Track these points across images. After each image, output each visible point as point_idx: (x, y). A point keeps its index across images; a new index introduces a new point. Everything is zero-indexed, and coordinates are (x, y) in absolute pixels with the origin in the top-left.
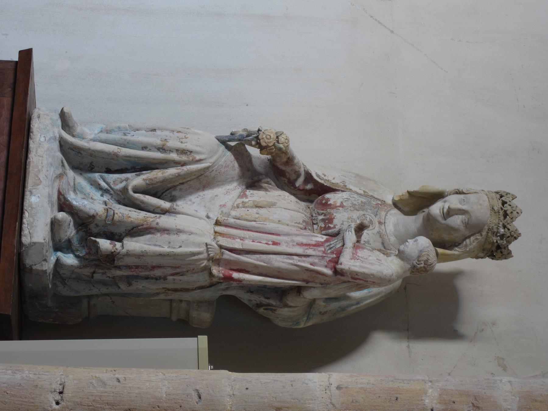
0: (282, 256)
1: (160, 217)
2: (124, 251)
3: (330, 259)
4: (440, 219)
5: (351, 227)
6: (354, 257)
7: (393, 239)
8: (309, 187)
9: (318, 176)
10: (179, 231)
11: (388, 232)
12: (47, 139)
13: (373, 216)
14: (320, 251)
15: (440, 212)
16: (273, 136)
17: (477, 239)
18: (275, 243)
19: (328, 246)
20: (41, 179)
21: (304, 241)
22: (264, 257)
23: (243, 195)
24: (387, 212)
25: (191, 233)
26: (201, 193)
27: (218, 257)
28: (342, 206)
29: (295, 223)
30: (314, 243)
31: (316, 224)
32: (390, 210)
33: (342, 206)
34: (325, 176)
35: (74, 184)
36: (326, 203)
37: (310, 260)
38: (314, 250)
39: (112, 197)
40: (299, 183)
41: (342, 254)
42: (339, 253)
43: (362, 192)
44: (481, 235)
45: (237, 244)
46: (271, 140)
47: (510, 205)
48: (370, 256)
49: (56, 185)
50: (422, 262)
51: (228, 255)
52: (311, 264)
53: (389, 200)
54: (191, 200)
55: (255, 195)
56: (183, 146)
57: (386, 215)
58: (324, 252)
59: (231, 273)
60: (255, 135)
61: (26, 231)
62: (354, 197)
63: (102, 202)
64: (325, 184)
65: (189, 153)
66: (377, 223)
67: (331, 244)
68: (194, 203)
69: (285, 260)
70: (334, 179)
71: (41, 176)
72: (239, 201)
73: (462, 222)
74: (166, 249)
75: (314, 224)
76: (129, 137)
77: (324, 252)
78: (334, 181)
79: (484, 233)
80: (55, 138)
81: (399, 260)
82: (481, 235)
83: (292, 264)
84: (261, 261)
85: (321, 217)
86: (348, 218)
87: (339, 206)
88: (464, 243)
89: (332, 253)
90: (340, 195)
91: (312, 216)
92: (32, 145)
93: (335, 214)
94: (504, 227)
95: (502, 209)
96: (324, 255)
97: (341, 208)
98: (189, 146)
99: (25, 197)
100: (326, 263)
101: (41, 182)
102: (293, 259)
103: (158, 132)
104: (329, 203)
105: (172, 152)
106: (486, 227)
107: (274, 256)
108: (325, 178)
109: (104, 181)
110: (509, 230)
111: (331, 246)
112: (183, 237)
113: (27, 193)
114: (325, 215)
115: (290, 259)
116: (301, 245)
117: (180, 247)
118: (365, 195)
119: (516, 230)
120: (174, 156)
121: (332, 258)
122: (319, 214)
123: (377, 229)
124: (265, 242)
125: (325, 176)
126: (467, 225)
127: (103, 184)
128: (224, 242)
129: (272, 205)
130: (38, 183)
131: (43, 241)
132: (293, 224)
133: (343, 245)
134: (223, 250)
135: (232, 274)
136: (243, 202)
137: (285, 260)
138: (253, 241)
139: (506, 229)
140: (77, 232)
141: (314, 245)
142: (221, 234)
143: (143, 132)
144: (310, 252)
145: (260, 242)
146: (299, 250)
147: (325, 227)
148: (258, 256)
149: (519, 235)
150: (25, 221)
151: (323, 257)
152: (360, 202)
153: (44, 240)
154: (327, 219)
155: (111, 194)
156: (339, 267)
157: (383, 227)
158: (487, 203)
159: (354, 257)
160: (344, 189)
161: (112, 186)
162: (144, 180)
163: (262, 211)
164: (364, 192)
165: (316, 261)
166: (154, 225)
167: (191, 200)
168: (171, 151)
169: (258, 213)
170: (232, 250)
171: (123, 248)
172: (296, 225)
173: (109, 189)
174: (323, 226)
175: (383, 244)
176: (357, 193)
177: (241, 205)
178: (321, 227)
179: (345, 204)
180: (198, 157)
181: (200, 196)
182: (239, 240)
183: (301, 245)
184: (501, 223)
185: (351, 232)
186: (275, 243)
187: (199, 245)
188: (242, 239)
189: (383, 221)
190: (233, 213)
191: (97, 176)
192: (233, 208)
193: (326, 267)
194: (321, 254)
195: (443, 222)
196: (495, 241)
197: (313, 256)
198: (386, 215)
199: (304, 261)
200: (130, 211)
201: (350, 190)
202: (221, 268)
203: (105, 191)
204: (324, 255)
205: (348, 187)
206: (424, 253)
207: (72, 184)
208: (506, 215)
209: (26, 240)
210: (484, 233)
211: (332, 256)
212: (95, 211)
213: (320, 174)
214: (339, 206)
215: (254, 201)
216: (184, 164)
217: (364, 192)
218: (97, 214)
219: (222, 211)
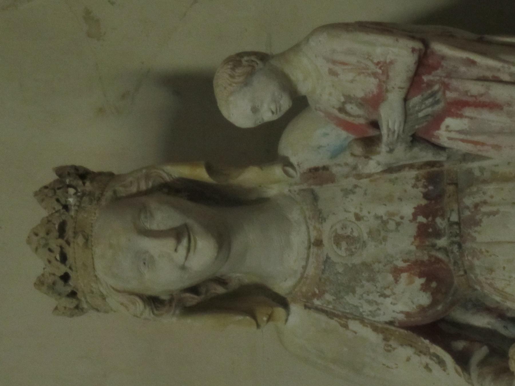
3: (434, 73)
4: (196, 227)
5: (388, 145)
7: (295, 215)
8: (460, 345)
9: (441, 363)
11: (304, 228)
13: (334, 258)
17: (124, 186)
19: (437, 102)
21: (486, 115)
24: (302, 277)
28: (397, 272)
30: (468, 112)
31: (451, 224)
32: (295, 287)
33: (397, 272)
34: (427, 367)
37: (475, 72)
40: (481, 352)
41: (411, 74)
42: (415, 83)
43: (354, 325)
44: (115, 192)
47: (50, 250)
48: (352, 82)
50: (244, 63)
52: (473, 63)
53: (297, 313)
57: (305, 268)
58: (446, 86)
62: (370, 302)
64: (427, 342)
66: (325, 242)
67: (432, 105)
73: (152, 215)
75: (458, 224)
77: (446, 86)
78: (408, 351)
79: (109, 194)
81: (293, 78)
82: (115, 192)
85: (442, 242)
86: (385, 239)
88: (150, 184)
89: (430, 85)
91: (460, 246)
93: (413, 248)
94: (66, 207)
95: (68, 243)
96: (446, 80)
97: (400, 264)
100: (444, 63)
104: (422, 281)
106: (103, 203)
108: (425, 359)
110: (58, 200)
111: (430, 100)
114: (434, 246)
116: (493, 106)
118: (344, 317)
119: (43, 200)
121: (429, 73)
122: (444, 250)
123: (326, 227)
126: (144, 209)
132: (502, 209)
133: (406, 100)
139: (63, 201)
141: (465, 104)
144: (476, 88)
146: (499, 93)
147: (434, 217)
149: (36, 194)
151: (449, 76)
152: (359, 291)
154: (429, 235)
156: (418, 45)
157: (314, 234)
158: (98, 250)
159: (385, 67)
160: (386, 330)
164: (346, 326)
165: (463, 69)
172: (494, 209)
174: (438, 220)
175: (315, 198)
176: (362, 320)
178: (443, 216)
179: (390, 278)
183: (493, 106)
184: (72, 213)
193: (443, 58)
194: (454, 83)
195: (190, 222)
196: (88, 184)
197: (468, 79)
201: (375, 329)
204: (446, 80)
205: (381, 336)
206: (241, 79)
210: (109, 194)
211: (431, 78)
217: (346, 326)
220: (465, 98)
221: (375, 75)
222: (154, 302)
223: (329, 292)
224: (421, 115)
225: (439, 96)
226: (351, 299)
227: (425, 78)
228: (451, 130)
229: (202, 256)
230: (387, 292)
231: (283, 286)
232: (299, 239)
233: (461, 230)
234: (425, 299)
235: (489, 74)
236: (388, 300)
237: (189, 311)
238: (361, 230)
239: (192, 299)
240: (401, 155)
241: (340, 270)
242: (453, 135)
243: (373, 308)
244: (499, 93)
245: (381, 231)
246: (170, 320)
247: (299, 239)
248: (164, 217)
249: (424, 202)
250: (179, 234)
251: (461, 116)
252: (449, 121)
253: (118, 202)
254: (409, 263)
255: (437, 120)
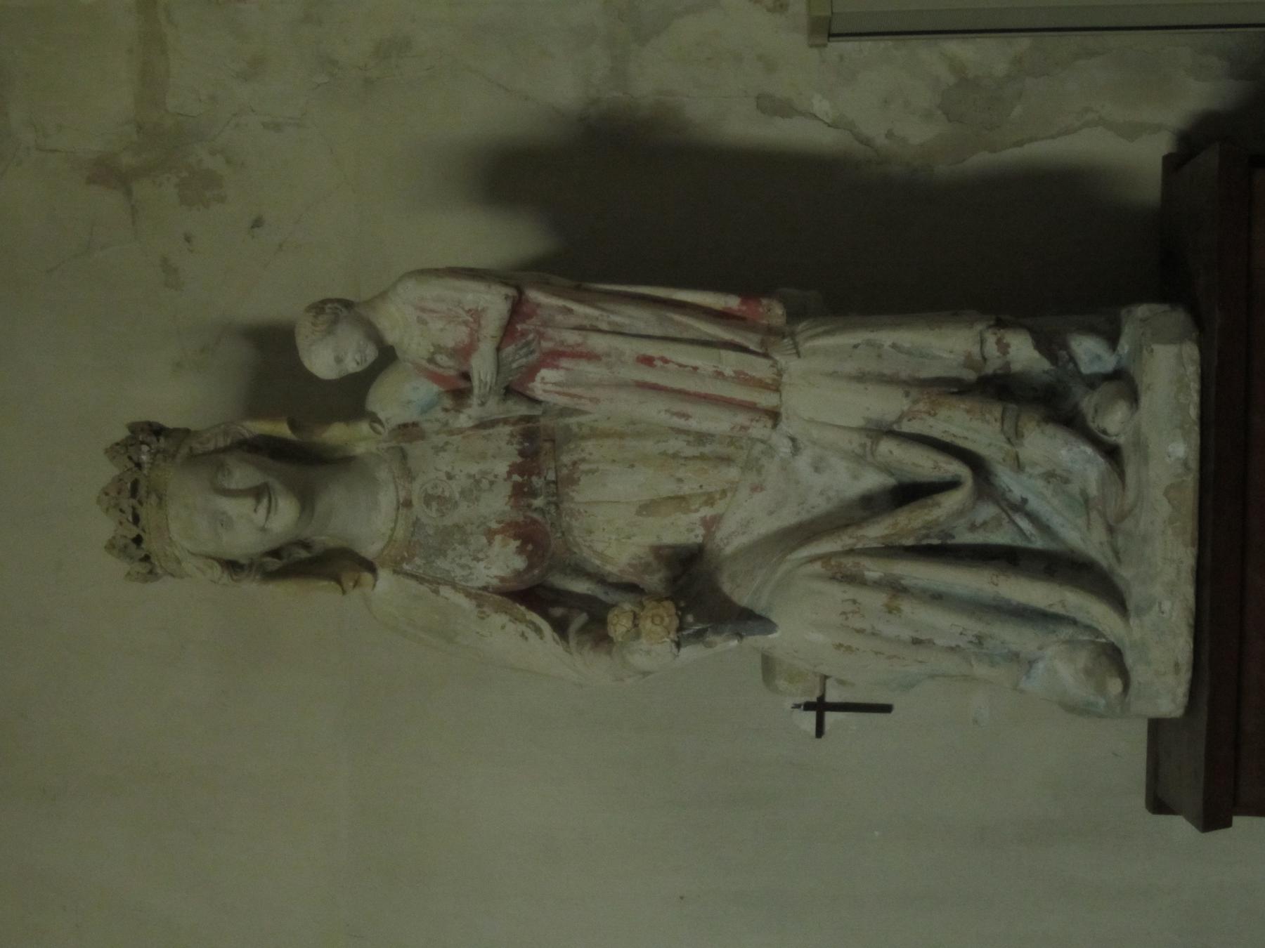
0: (634, 331)
1: (899, 420)
2: (979, 327)
4: (276, 485)
6: (477, 315)
7: (383, 474)
8: (558, 612)
9: (538, 630)
10: (861, 378)
11: (392, 487)
12: (1156, 608)
13: (424, 520)
14: (551, 339)
15: (276, 506)
16: (647, 625)
17: (201, 443)
18: (648, 361)
19: (532, 352)
20: (1165, 501)
22: (672, 332)
23: (710, 524)
25: (834, 375)
26: (805, 517)
27: (772, 339)
28: (490, 534)
29: (597, 470)
30: (564, 363)
31: (548, 483)
32: (383, 550)
33: (490, 534)
34: (523, 635)
35: (1088, 514)
36: (525, 543)
37: (573, 321)
38: (562, 343)
39: (1003, 494)
42: (508, 332)
43: (446, 591)
44: (191, 449)
45: (731, 362)
46: (650, 614)
48: (442, 330)
49: (1131, 495)
50: (328, 311)
51: (752, 341)
52: (570, 311)
54: (829, 499)
55: (680, 530)
56: (852, 592)
57: (393, 530)
58: (541, 336)
59: (744, 308)
60: (685, 633)
61: (1192, 371)
62: (462, 567)
63: (1028, 469)
65: (839, 576)
66: (415, 502)
67: (526, 355)
68: (822, 493)
69: (627, 321)
70: (503, 627)
71: (1165, 509)
72: (720, 507)
74: (886, 337)
75: (555, 483)
76: (974, 626)
77: (541, 336)
79: (184, 451)
80: (1141, 612)
82: (191, 449)
83: (613, 312)
84: (679, 324)
85: (538, 502)
86: (477, 499)
87: (496, 532)
88: (229, 441)
90: (495, 571)
92: (1189, 591)
93: (508, 508)
94: (139, 465)
96: (542, 329)
97: (494, 526)
98: (839, 593)
99: (1198, 456)
101: (1166, 494)
102: (609, 323)
103: (906, 634)
104: (518, 543)
105: (875, 582)
107: (650, 332)
108: (522, 627)
109: (1020, 530)
110: (130, 458)
111: (525, 350)
112: (850, 367)
113: (1194, 465)
114: (529, 506)
115: (617, 324)
116: (591, 357)
117: (856, 346)
120: (874, 570)
121: (524, 322)
123: (416, 486)
124: (670, 366)
125: (523, 635)
127: (1024, 524)
128: (760, 368)
129: (648, 508)
130: (606, 593)
131: (1156, 347)
134: (759, 350)
135: (743, 303)
136: (712, 505)
137: (627, 321)
138: (695, 368)
139: (135, 458)
140: (1076, 406)
141: (562, 354)
142: (761, 385)
143: (940, 642)
144: (572, 338)
145: (680, 365)
146: (598, 343)
147: (530, 475)
148: (686, 335)
150: (1195, 398)
151: (545, 324)
153: (1152, 351)
155: (1006, 500)
156: (511, 292)
157: (402, 494)
159: (477, 315)
160: (479, 596)
161: (1004, 515)
162: (938, 505)
163: (668, 488)
165: (559, 318)
166: (914, 392)
167: (829, 499)
168: (878, 585)
169: (680, 480)
170: (745, 350)
171: (981, 333)
173: (1010, 512)
174: (534, 479)
176: (454, 586)
177: (718, 496)
178: (539, 474)
179: (484, 540)
180: (817, 567)
181: (808, 511)
182: (728, 372)
183: (591, 357)
184: (145, 472)
185: (480, 380)
186: (648, 361)
187: (814, 352)
188: (719, 375)
189: (403, 511)
190: (733, 473)
191: (1039, 543)
192: (734, 487)
193: (539, 305)
194: (550, 332)
195: (272, 481)
198: (393, 530)
199: (586, 316)
200: (966, 438)
201: (468, 594)
202: (765, 322)
203: (1020, 507)
205: (474, 602)
207: (1094, 514)
208: (134, 491)
209: (1191, 351)
211: (525, 326)
212: (1043, 432)
213: (531, 635)
214: (496, 532)
215: (687, 511)
216: (851, 552)
217: (436, 592)
218: (1038, 425)
219: (759, 472)
220: (561, 349)
221: (466, 323)
222: (232, 566)
223: (419, 555)
224: (514, 365)
225: (533, 346)
226: (442, 563)
227: (519, 327)
228: (546, 382)
229: (283, 517)
230: (480, 556)
231: (370, 550)
232: (387, 499)
233: (560, 487)
234: (520, 563)
235: (586, 323)
236: (482, 565)
237: (271, 576)
238: (453, 489)
239: (273, 564)
240: (494, 408)
241: (431, 532)
242: (549, 387)
243: (465, 573)
244: (598, 343)
245: (474, 490)
246: (251, 587)
247: (387, 499)
248: (243, 475)
249: (519, 460)
250: (258, 493)
251: (557, 367)
252: (546, 374)
253: (194, 459)
254: (1046, 365)
255: (531, 372)
